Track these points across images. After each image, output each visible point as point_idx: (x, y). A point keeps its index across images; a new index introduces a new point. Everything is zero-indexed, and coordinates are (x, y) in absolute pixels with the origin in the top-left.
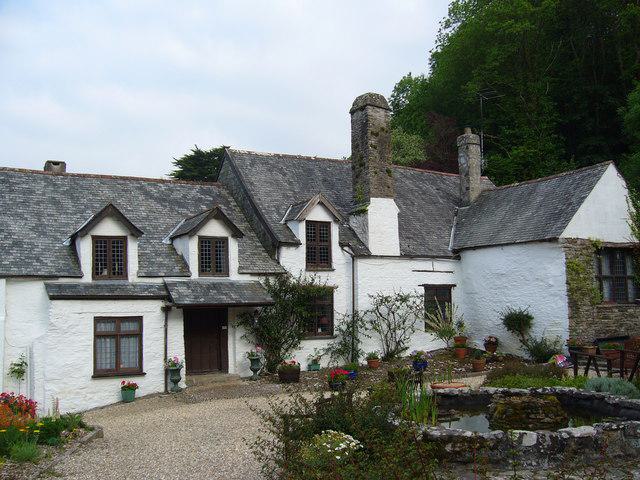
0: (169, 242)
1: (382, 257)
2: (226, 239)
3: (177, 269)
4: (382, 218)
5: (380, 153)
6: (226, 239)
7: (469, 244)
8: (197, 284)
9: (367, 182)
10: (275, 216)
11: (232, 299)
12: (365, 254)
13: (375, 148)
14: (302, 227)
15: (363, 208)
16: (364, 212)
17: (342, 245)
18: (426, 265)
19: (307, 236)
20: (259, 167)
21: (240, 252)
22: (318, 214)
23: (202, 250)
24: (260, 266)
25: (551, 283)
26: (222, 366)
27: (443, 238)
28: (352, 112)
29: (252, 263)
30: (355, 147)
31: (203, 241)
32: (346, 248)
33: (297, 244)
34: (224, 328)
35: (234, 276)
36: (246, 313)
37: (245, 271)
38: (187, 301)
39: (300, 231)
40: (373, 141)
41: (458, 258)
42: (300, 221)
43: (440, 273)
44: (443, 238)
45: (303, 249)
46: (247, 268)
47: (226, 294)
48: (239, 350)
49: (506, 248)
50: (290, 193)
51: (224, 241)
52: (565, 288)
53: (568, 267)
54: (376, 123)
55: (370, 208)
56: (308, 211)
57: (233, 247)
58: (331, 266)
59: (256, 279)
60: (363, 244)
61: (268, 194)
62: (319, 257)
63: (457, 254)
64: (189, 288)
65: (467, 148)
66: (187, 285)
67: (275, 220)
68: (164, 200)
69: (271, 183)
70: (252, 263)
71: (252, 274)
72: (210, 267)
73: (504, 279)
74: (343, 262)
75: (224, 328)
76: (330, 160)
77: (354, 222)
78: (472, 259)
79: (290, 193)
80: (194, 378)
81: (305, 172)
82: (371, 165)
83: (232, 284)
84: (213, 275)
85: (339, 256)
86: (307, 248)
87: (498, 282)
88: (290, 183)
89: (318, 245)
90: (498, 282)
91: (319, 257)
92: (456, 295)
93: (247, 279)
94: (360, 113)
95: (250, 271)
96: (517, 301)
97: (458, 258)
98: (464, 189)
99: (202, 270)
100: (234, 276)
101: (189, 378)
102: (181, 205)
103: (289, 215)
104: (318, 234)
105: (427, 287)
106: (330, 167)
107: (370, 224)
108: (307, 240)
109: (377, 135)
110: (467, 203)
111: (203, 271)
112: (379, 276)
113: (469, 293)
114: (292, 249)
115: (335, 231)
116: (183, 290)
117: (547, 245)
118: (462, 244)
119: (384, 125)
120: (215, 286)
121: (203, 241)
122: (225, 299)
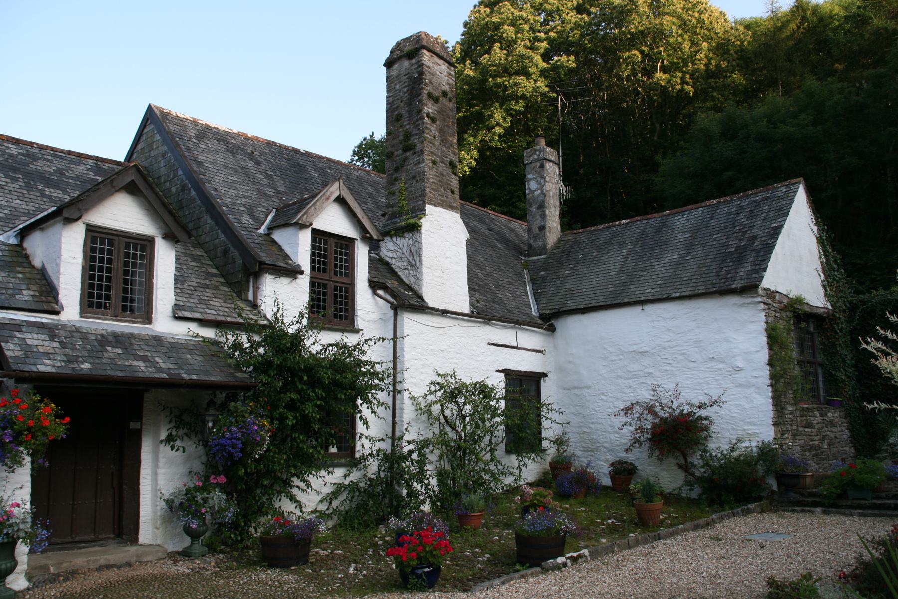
0: (13, 241)
1: (444, 313)
2: (150, 241)
3: (26, 295)
4: (444, 241)
5: (441, 130)
6: (150, 241)
7: (571, 305)
8: (75, 331)
9: (419, 177)
10: (247, 220)
11: (160, 370)
12: (419, 307)
13: (433, 120)
14: (305, 237)
15: (412, 221)
16: (415, 228)
17: (374, 285)
18: (506, 335)
19: (313, 261)
20: (213, 144)
21: (179, 279)
22: (332, 220)
23: (93, 259)
24: (217, 309)
25: (740, 364)
26: (125, 526)
27: (520, 296)
28: (389, 64)
29: (201, 301)
30: (393, 117)
31: (97, 237)
32: (380, 292)
33: (293, 272)
34: (133, 425)
35: (164, 324)
36: (188, 402)
37: (187, 314)
38: (45, 367)
39: (300, 248)
40: (429, 108)
41: (552, 329)
42: (303, 226)
43: (523, 349)
44: (520, 296)
45: (304, 282)
46: (191, 310)
47: (144, 359)
48: (161, 473)
49: (649, 308)
50: (270, 191)
51: (145, 244)
52: (766, 371)
53: (770, 337)
54: (434, 80)
55: (426, 224)
56: (318, 211)
57: (165, 260)
58: (352, 322)
59: (209, 333)
60: (410, 288)
61: (231, 185)
62: (331, 303)
63: (547, 322)
64: (53, 337)
65: (542, 166)
66: (51, 331)
67: (253, 228)
68: (15, 170)
69: (236, 171)
70: (201, 301)
71: (203, 323)
72: (108, 297)
73: (646, 361)
74: (374, 317)
75: (133, 425)
76: (329, 160)
77: (389, 249)
78: (576, 328)
79: (270, 191)
80: (55, 561)
81: (296, 176)
82: (428, 148)
83: (158, 341)
84: (116, 317)
85: (368, 306)
86: (312, 284)
87: (634, 367)
88: (269, 177)
89: (332, 279)
90: (634, 367)
91: (331, 303)
92: (549, 391)
93: (181, 331)
94: (406, 63)
95: (197, 316)
96: (687, 390)
97: (552, 329)
98: (536, 230)
99: (93, 301)
100: (164, 324)
101: (41, 559)
102: (49, 182)
103: (272, 221)
104: (331, 253)
105: (507, 372)
106: (330, 168)
107: (425, 252)
108: (313, 268)
109: (436, 100)
110: (543, 250)
111: (91, 305)
112: (437, 348)
113: (572, 389)
114: (285, 280)
115: (362, 255)
116: (35, 340)
117: (734, 300)
118: (555, 306)
119: (446, 88)
120: (118, 339)
121: (97, 237)
122: (141, 368)
